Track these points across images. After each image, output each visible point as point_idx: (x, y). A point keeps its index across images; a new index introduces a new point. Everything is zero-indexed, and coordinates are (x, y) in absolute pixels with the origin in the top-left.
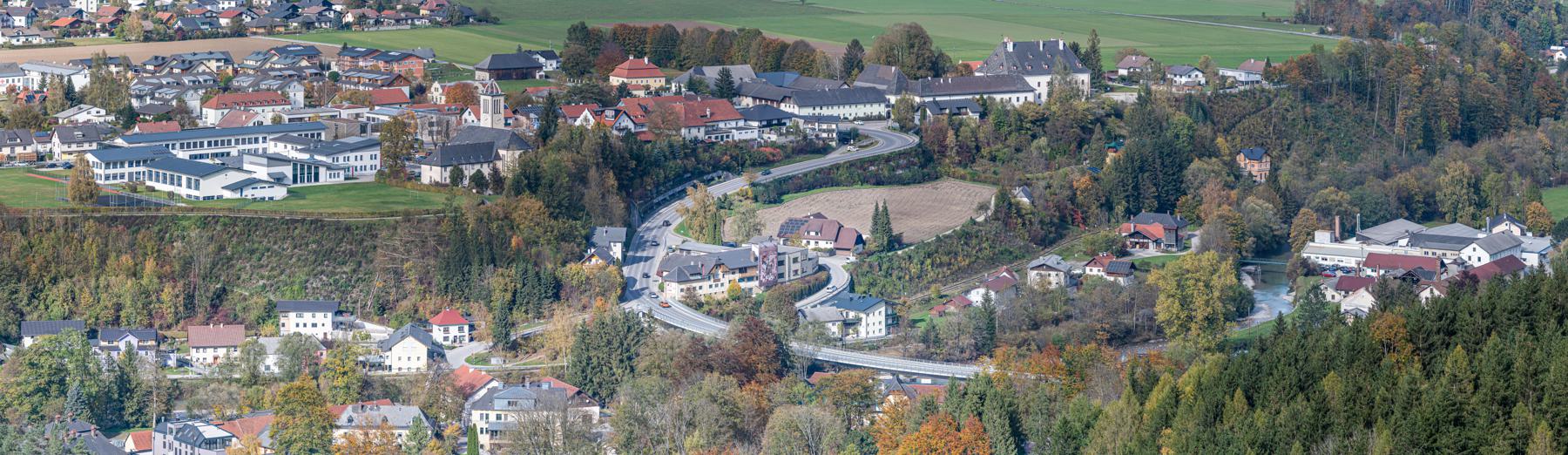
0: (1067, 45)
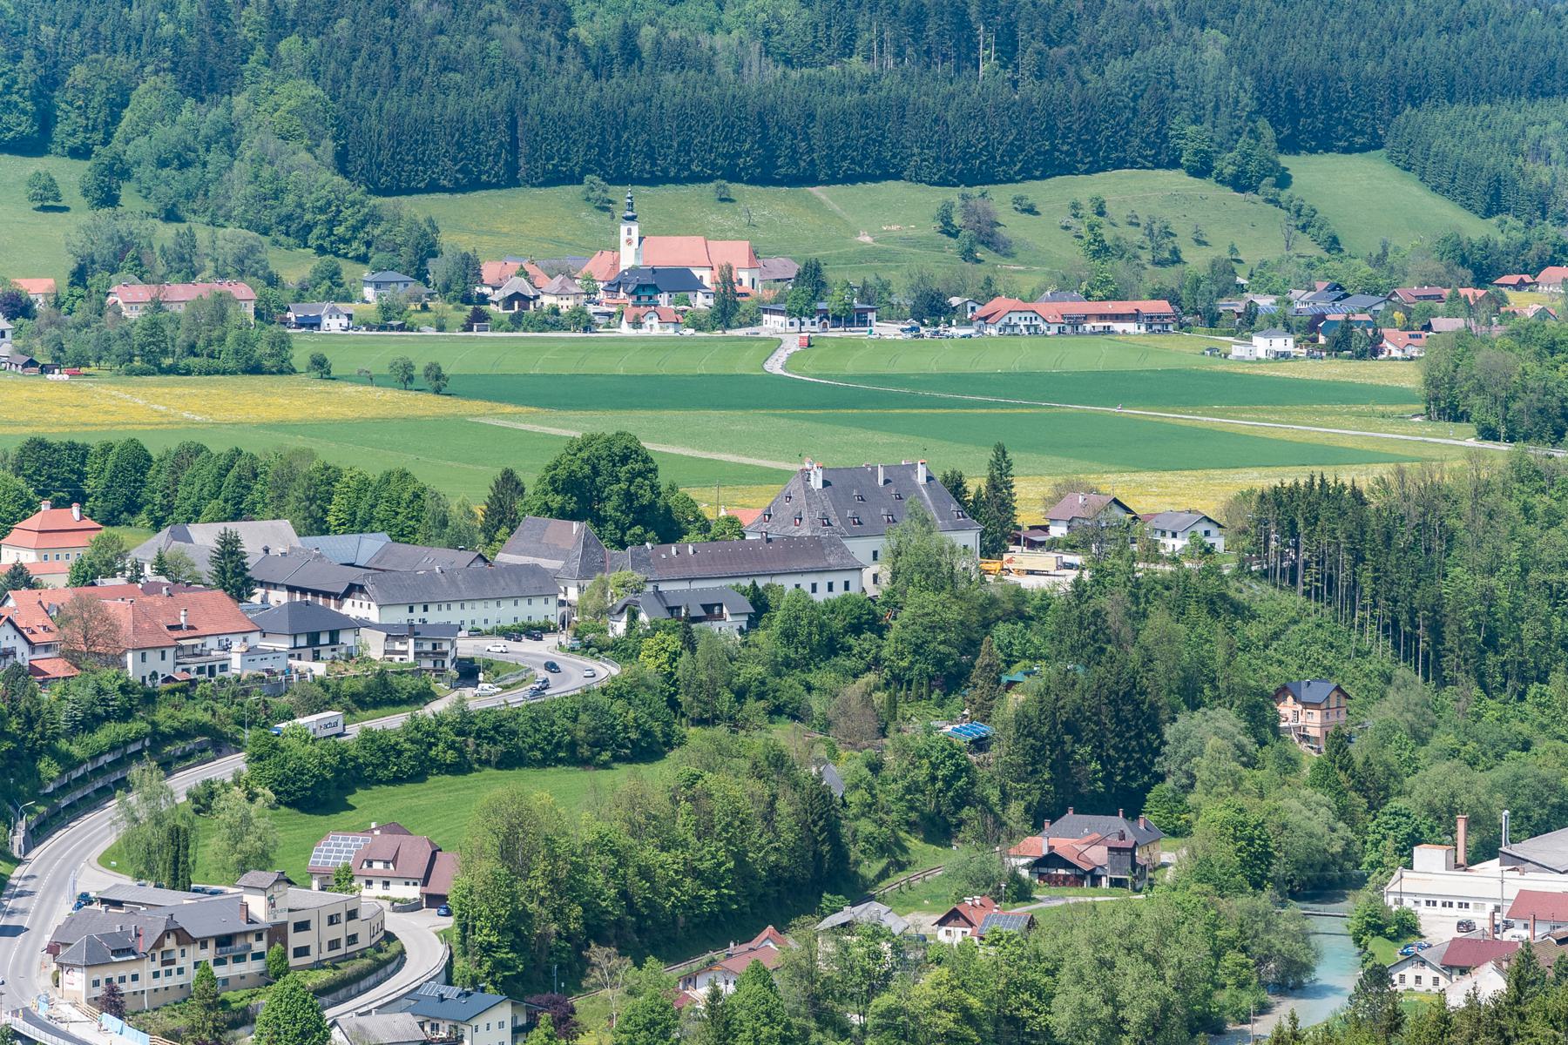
0: (938, 477)
